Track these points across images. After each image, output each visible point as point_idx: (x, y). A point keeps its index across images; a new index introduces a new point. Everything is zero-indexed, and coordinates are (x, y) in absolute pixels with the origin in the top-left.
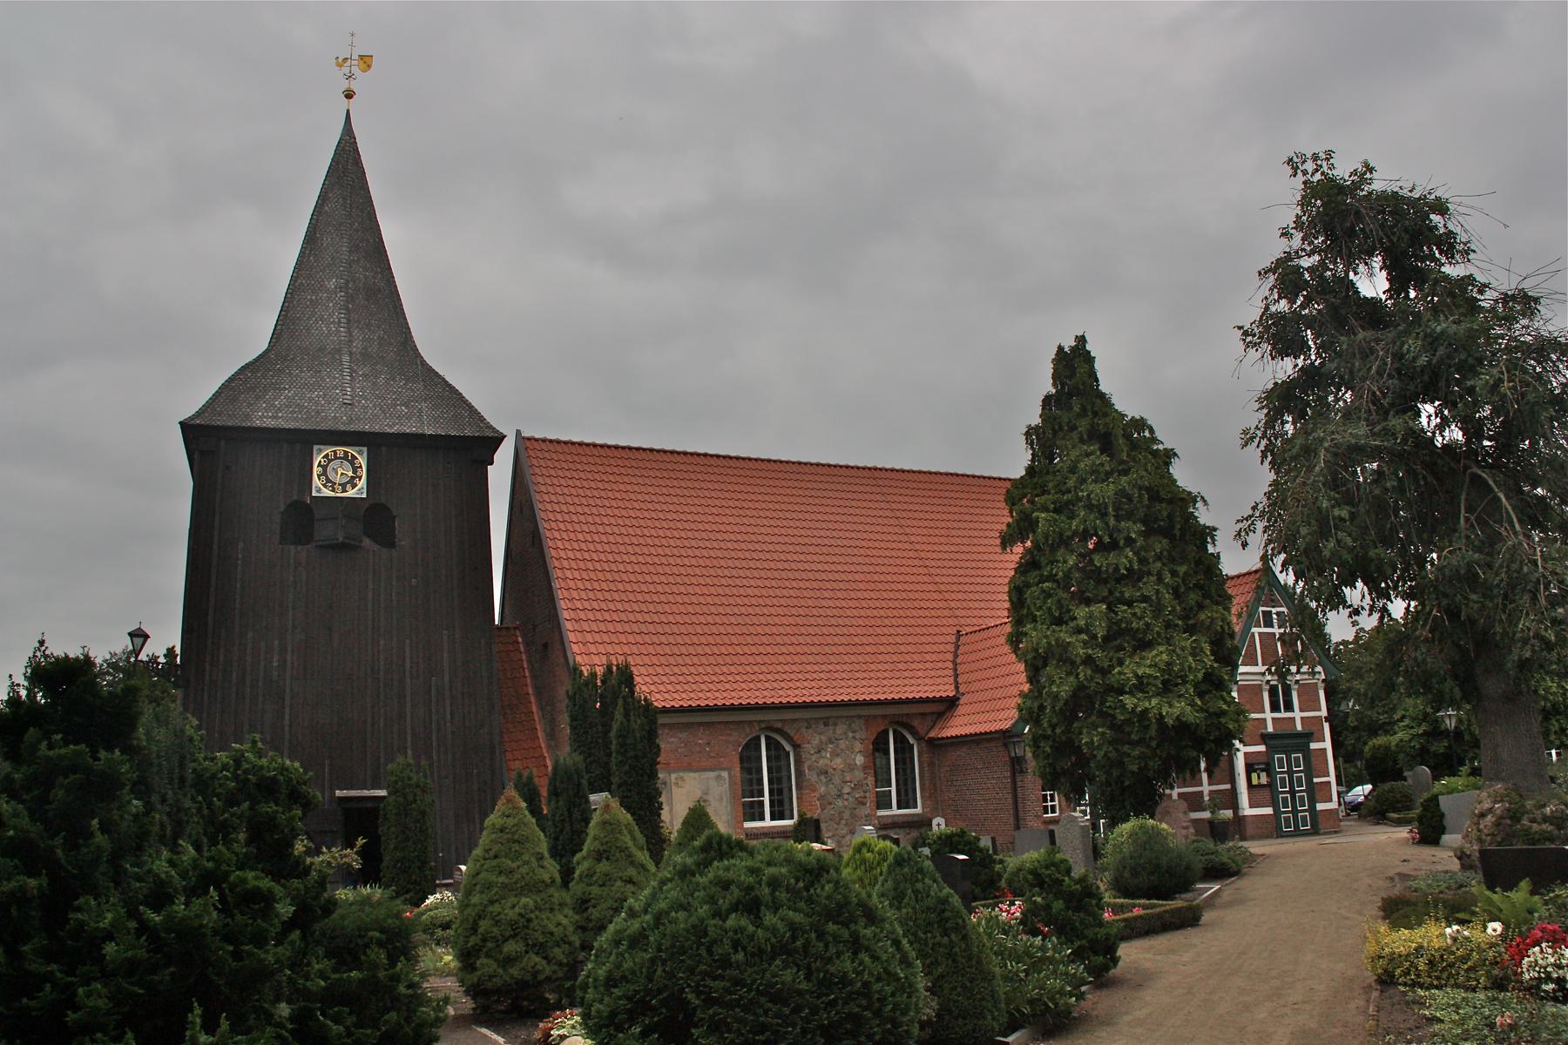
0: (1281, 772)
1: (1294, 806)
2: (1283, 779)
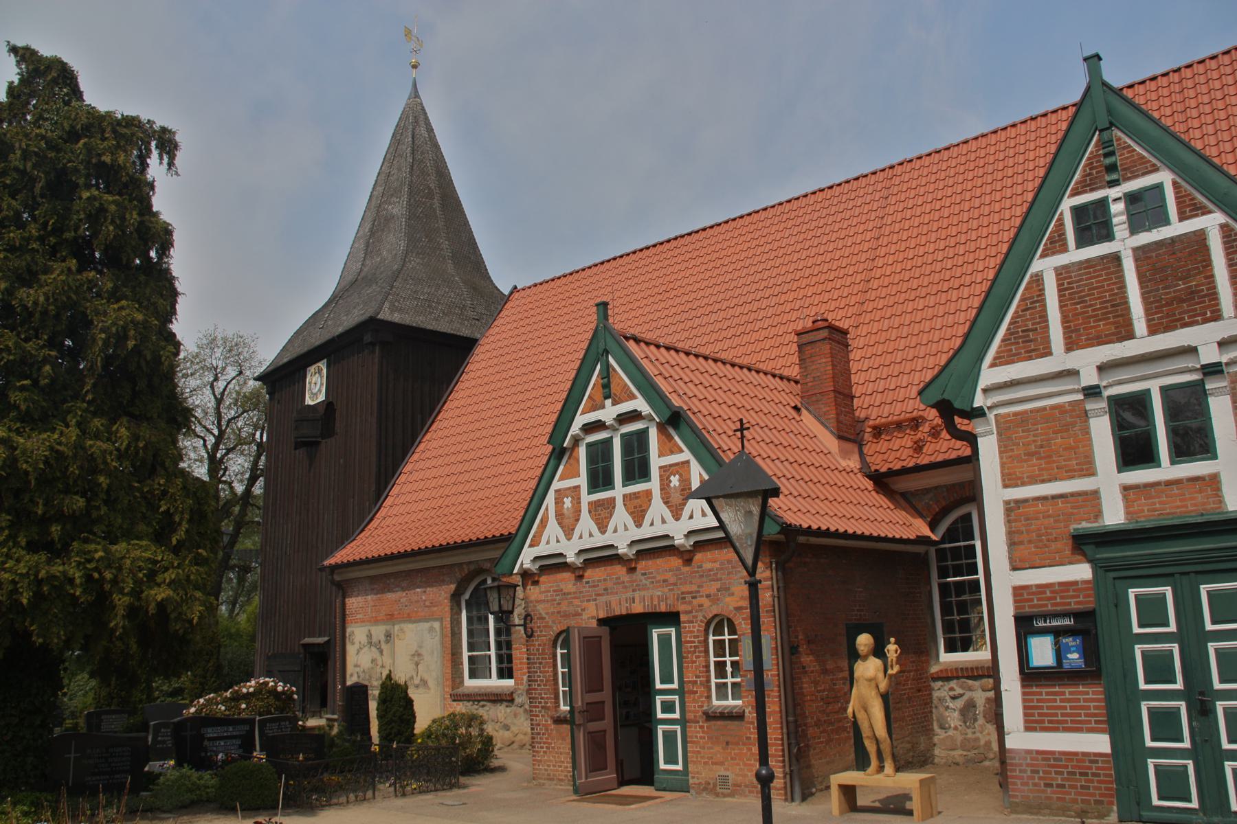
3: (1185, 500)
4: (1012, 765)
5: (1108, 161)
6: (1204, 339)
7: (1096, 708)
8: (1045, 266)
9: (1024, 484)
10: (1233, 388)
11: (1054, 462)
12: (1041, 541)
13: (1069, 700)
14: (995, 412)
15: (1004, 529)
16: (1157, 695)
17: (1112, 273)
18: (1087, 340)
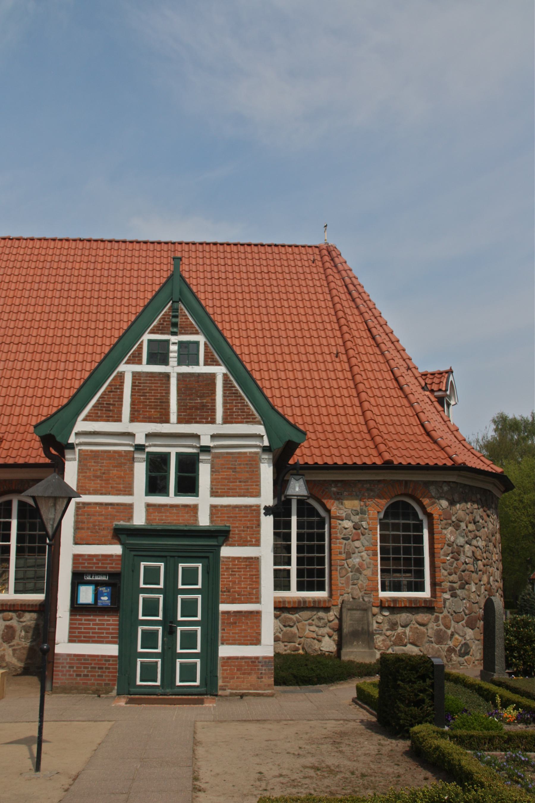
3: (179, 516)
4: (57, 663)
5: (174, 320)
6: (205, 432)
7: (113, 629)
8: (127, 369)
9: (90, 494)
10: (213, 461)
11: (110, 483)
12: (95, 529)
14: (79, 448)
16: (148, 623)
17: (164, 384)
18: (143, 418)
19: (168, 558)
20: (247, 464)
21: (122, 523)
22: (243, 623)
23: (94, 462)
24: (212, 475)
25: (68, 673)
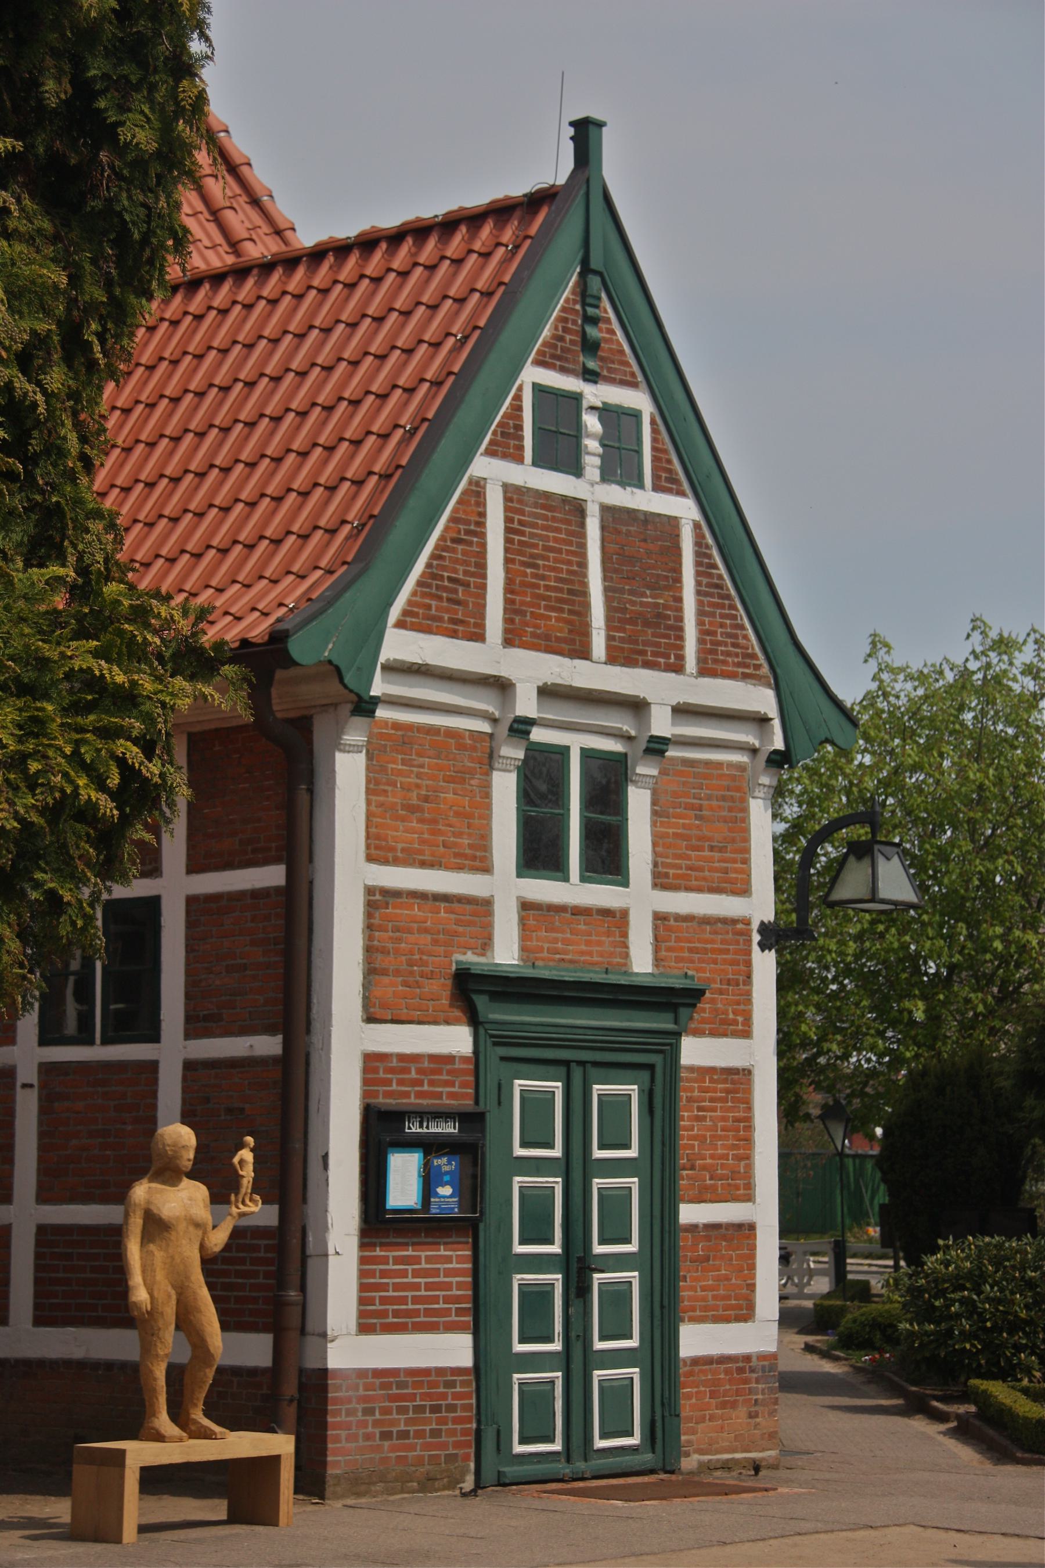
0: (528, 1171)
1: (576, 1336)
2: (615, 1205)
9: (396, 862)
13: (426, 1273)
15: (361, 943)
16: (533, 1261)
19: (588, 1066)
20: (724, 798)
21: (470, 958)
22: (722, 1257)
23: (404, 762)
24: (654, 824)
25: (361, 1431)
